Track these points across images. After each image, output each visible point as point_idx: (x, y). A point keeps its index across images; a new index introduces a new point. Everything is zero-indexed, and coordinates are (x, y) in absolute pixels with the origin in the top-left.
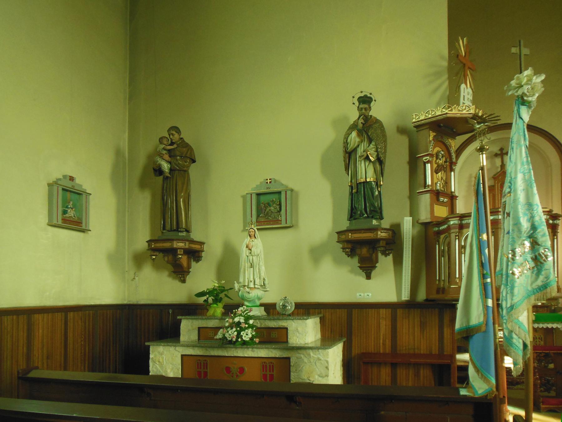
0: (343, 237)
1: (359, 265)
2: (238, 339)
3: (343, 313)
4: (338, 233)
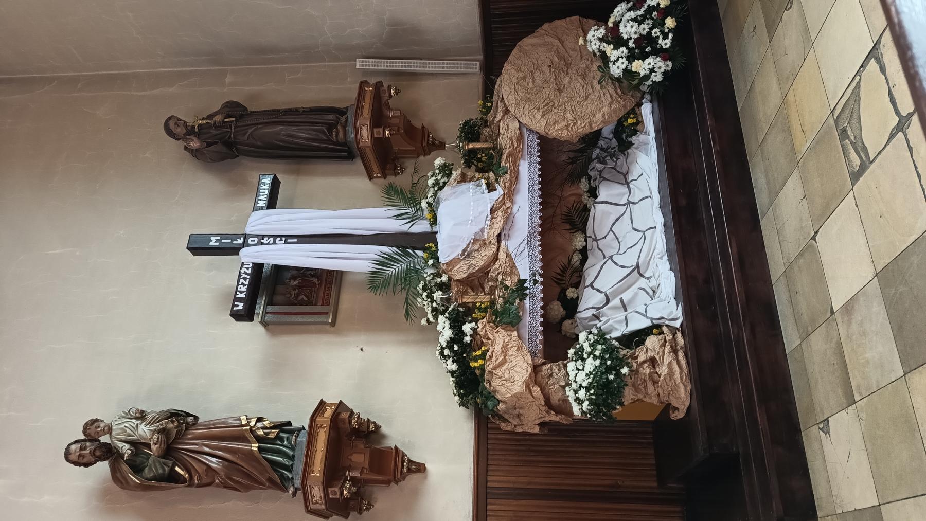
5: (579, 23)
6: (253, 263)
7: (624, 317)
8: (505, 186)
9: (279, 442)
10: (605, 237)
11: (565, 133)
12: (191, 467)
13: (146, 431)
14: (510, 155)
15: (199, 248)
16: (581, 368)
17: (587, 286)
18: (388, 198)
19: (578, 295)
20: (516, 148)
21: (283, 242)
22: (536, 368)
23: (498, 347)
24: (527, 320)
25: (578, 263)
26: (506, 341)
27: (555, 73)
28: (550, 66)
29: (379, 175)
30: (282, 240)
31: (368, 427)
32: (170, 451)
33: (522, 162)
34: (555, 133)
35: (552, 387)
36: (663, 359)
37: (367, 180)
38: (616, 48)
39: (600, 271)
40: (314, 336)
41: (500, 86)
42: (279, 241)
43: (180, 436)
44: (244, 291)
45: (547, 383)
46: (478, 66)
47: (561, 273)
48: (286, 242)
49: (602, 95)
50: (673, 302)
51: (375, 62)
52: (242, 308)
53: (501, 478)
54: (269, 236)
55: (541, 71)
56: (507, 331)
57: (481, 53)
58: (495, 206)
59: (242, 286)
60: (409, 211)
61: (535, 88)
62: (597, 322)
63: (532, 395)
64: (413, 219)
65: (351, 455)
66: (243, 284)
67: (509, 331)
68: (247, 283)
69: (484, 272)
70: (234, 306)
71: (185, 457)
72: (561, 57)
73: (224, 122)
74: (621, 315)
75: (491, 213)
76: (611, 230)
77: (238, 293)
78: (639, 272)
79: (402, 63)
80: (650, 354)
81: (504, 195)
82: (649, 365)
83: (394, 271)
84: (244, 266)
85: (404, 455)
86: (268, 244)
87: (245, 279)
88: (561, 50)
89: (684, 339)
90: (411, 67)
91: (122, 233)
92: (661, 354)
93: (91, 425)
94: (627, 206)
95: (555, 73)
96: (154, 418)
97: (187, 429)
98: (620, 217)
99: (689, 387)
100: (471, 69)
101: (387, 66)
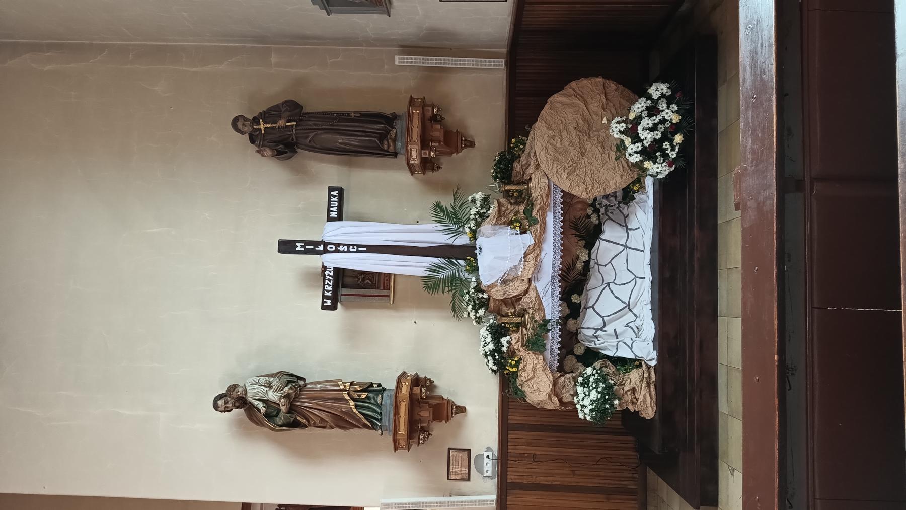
0: (402, 442)
1: (444, 421)
2: (676, 104)
3: (512, 435)
4: (395, 450)
8: (535, 236)
11: (584, 193)
12: (308, 417)
14: (540, 209)
15: (287, 247)
16: (587, 393)
17: (589, 307)
18: (436, 215)
20: (545, 204)
21: (355, 250)
22: (555, 383)
24: (549, 346)
26: (535, 362)
31: (426, 382)
32: (292, 409)
33: (548, 213)
36: (641, 390)
37: (409, 174)
38: (633, 143)
39: (600, 296)
40: (378, 310)
42: (352, 249)
43: (297, 396)
44: (330, 291)
46: (503, 64)
47: (566, 271)
48: (358, 251)
49: (616, 167)
50: (651, 344)
51: (412, 59)
52: (330, 304)
53: (518, 418)
54: (344, 245)
56: (535, 354)
59: (328, 286)
64: (457, 233)
65: (420, 412)
66: (328, 284)
68: (331, 284)
69: (518, 298)
71: (304, 411)
73: (286, 126)
74: (613, 341)
75: (524, 257)
76: (610, 262)
77: (325, 292)
78: (629, 308)
79: (436, 60)
80: (632, 385)
83: (442, 276)
84: (327, 269)
85: (453, 404)
86: (344, 252)
87: (329, 280)
88: (586, 113)
89: (656, 376)
90: (444, 64)
91: (207, 215)
92: (640, 386)
97: (301, 390)
98: (618, 254)
100: (497, 66)
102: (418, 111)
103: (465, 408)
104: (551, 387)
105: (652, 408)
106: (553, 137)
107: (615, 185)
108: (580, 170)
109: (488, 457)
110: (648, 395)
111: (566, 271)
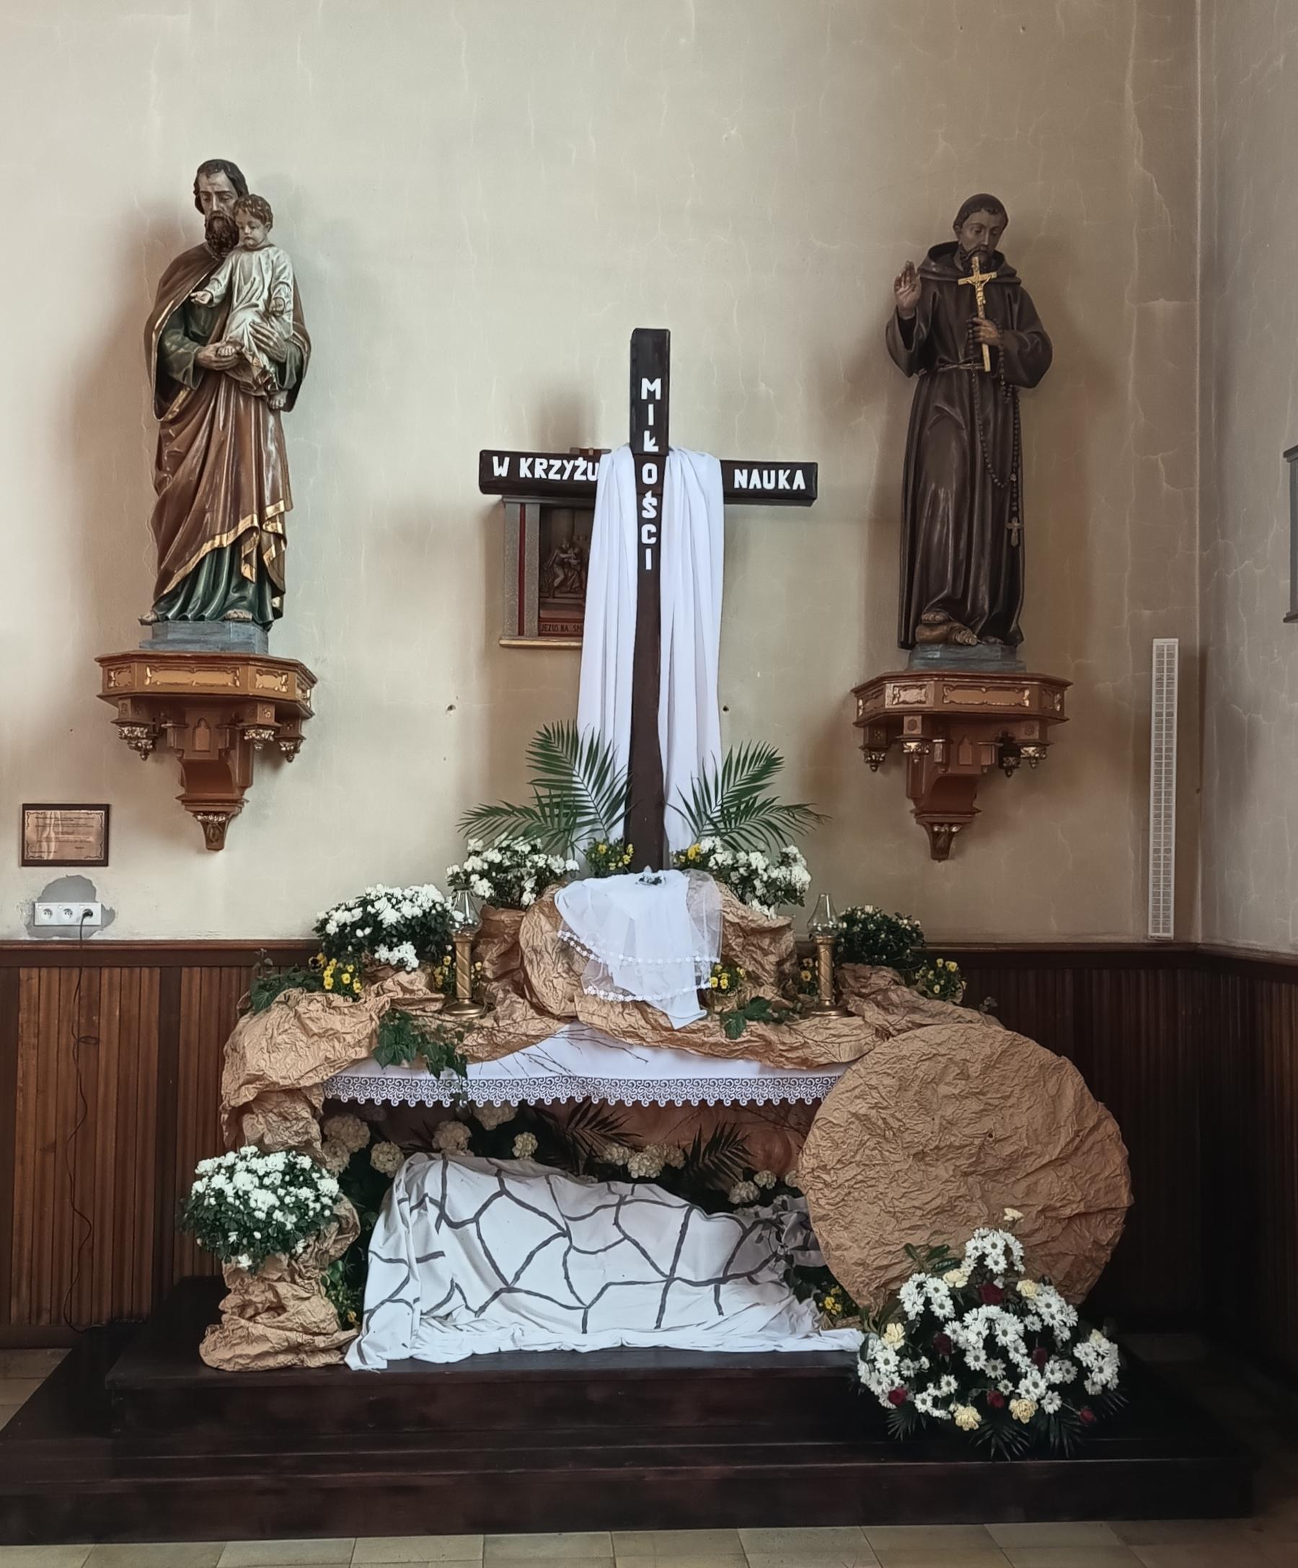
0: (122, 680)
1: (182, 791)
3: (148, 978)
5: (1102, 1207)
6: (596, 482)
7: (403, 1256)
8: (694, 1032)
9: (233, 584)
10: (616, 1223)
12: (186, 420)
13: (240, 330)
14: (769, 1043)
16: (267, 1181)
17: (501, 1183)
19: (518, 1158)
21: (645, 540)
22: (294, 1093)
23: (335, 1022)
24: (394, 1074)
25: (609, 1157)
26: (348, 1038)
27: (967, 1146)
28: (991, 1136)
29: (861, 713)
30: (649, 538)
31: (289, 740)
32: (208, 376)
34: (813, 1141)
35: (261, 1119)
36: (279, 1328)
37: (855, 682)
38: (953, 1294)
39: (534, 1210)
40: (483, 607)
41: (959, 1019)
42: (649, 531)
43: (242, 390)
44: (533, 473)
45: (271, 1111)
47: (599, 1118)
48: (642, 547)
49: (888, 1248)
50: (404, 1354)
53: (195, 994)
54: (659, 508)
55: (982, 1113)
56: (370, 1036)
57: (1208, 940)
58: (649, 1010)
59: (545, 466)
60: (713, 804)
61: (935, 1100)
62: (414, 1203)
63: (242, 1085)
64: (698, 815)
66: (550, 467)
67: (370, 1043)
68: (553, 476)
69: (522, 987)
70: (502, 455)
72: (1016, 1161)
74: (411, 1250)
76: (626, 1237)
77: (530, 460)
78: (501, 1291)
80: (291, 1304)
81: (672, 1029)
82: (272, 1302)
85: (230, 816)
86: (640, 508)
87: (561, 470)
88: (1032, 1164)
89: (319, 1368)
90: (1158, 772)
92: (289, 1325)
93: (251, 213)
94: (665, 1276)
95: (967, 1146)
96: (268, 337)
98: (648, 1258)
99: (226, 1367)
101: (1159, 714)
102: (1027, 703)
103: (220, 848)
104: (282, 1082)
105: (230, 1359)
106: (964, 1075)
107: (838, 1247)
108: (874, 1149)
109: (88, 914)
110: (265, 1347)
111: (599, 1118)
